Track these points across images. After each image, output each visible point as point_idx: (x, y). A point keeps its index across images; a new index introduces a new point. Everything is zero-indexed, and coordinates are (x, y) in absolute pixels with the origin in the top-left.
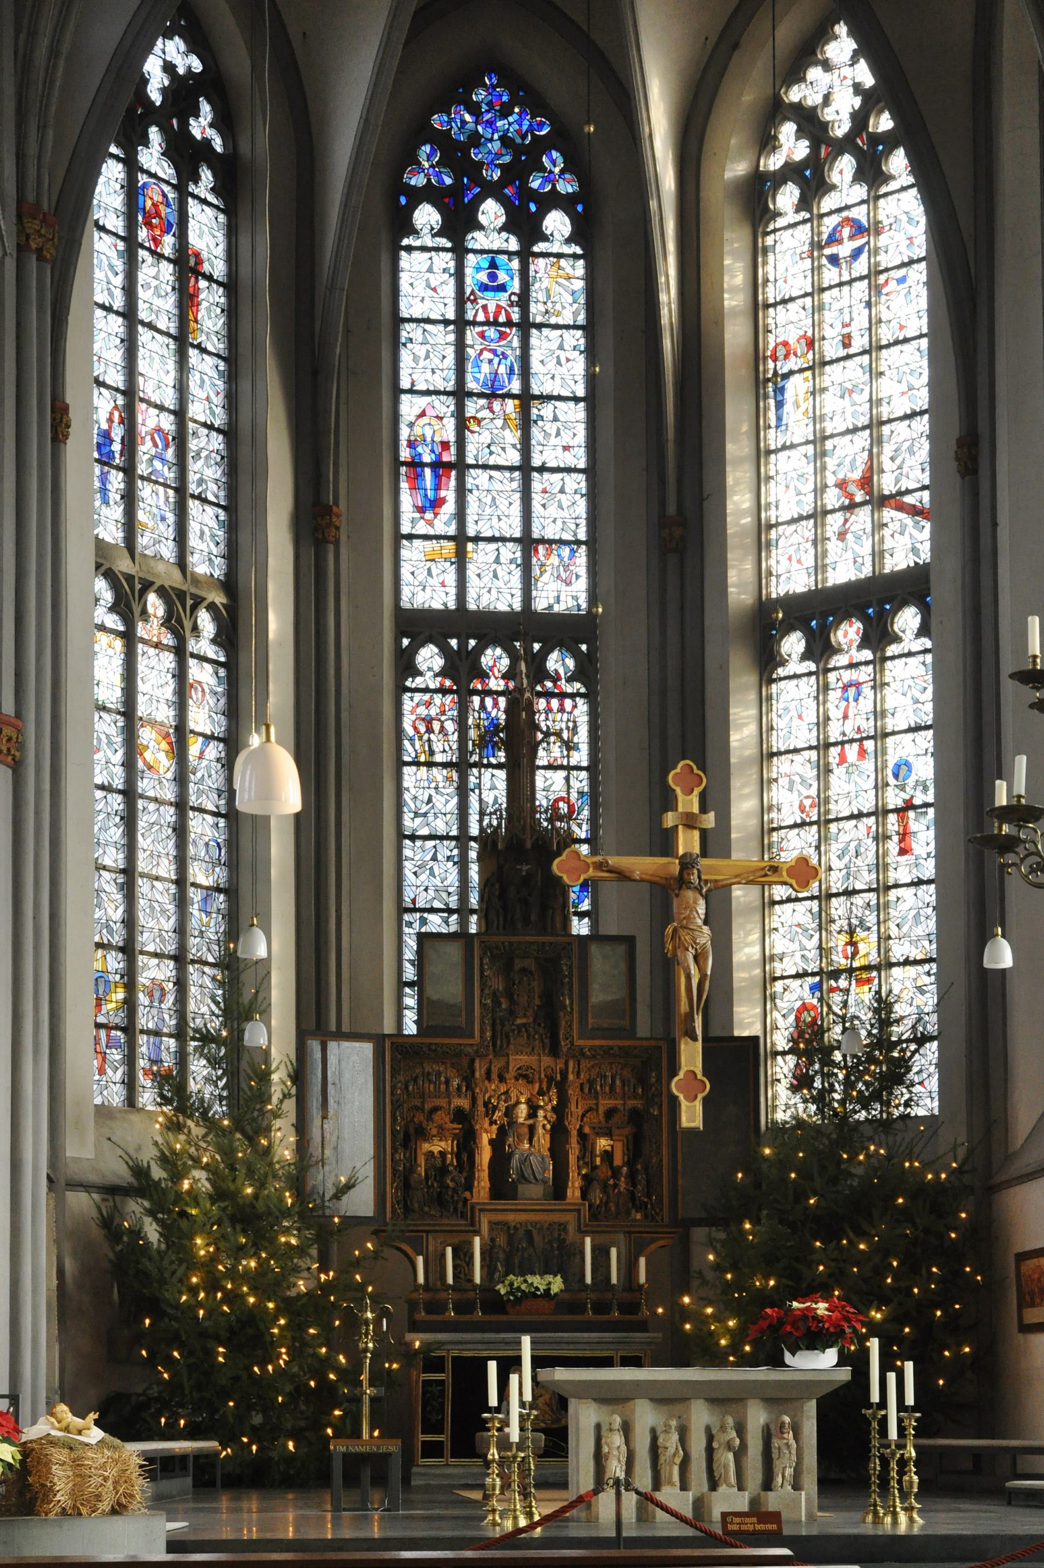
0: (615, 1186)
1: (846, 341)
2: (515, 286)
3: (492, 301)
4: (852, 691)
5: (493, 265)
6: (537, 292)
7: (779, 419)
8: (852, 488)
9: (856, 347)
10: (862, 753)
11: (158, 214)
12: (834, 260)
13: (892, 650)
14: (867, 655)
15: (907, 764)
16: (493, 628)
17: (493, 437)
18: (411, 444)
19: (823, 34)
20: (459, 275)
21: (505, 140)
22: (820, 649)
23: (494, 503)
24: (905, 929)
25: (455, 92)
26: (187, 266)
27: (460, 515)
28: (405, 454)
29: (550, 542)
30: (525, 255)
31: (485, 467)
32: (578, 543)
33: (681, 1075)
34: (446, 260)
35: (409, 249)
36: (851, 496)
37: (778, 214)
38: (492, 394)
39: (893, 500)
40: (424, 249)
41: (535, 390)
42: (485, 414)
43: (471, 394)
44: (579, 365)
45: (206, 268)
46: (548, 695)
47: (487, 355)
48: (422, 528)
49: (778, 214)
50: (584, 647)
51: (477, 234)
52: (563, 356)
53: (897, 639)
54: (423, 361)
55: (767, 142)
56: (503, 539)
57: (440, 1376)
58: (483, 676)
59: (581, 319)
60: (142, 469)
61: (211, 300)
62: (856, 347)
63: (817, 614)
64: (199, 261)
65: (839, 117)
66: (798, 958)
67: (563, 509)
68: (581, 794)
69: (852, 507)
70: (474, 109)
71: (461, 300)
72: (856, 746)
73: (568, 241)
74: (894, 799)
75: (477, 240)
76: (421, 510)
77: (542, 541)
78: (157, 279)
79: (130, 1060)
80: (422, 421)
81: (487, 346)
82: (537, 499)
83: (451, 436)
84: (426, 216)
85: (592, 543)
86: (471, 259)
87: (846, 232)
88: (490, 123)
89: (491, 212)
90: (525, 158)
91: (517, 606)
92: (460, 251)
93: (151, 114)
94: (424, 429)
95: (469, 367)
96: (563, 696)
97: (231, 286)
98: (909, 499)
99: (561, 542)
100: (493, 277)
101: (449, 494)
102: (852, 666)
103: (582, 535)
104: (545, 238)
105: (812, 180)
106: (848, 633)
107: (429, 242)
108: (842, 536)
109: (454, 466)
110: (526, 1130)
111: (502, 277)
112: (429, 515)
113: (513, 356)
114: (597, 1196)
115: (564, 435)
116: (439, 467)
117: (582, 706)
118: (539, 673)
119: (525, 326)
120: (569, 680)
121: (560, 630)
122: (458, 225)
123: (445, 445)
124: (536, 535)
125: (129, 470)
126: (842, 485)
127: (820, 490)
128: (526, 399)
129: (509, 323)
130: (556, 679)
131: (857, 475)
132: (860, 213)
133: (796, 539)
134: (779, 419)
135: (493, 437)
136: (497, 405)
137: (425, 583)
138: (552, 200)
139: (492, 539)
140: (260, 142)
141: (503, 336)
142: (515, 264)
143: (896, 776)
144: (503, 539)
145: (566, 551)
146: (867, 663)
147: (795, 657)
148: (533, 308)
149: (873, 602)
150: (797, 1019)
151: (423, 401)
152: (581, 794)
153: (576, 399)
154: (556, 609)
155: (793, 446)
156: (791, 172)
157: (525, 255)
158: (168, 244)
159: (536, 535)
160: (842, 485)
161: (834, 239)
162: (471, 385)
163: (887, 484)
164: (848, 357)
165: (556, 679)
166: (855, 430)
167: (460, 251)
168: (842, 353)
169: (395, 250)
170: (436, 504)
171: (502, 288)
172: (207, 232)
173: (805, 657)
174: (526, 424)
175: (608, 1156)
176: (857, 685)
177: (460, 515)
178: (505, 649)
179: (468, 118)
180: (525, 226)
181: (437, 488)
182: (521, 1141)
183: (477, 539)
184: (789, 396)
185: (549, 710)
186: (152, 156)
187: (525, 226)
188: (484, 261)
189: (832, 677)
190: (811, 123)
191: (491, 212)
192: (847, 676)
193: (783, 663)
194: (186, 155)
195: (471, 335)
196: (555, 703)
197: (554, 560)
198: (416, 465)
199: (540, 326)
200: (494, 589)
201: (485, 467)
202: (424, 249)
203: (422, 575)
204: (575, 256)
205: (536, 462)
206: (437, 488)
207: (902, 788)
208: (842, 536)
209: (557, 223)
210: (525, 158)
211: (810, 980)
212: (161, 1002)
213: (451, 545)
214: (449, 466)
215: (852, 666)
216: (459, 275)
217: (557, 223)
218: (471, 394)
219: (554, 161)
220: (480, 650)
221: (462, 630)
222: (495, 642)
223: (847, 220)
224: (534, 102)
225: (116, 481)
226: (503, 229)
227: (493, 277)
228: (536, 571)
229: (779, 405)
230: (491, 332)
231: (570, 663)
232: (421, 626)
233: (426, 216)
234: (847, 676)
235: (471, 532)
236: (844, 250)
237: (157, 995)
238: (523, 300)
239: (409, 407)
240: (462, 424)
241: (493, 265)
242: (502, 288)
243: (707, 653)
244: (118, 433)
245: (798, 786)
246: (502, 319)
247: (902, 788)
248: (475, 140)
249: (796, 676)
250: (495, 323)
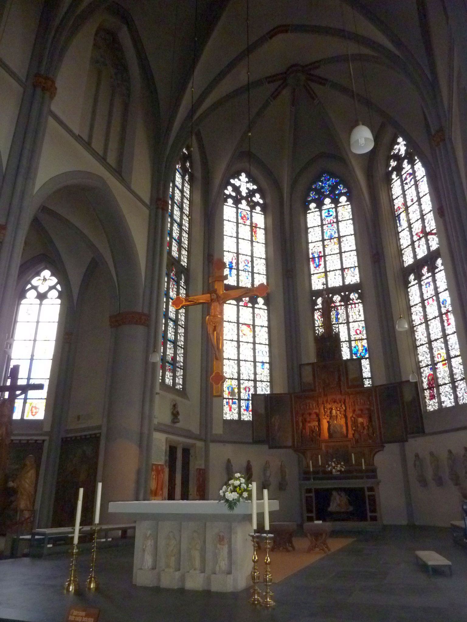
0: (363, 432)
1: (412, 200)
2: (334, 214)
3: (329, 219)
4: (428, 285)
5: (329, 211)
6: (339, 214)
7: (400, 224)
8: (419, 234)
9: (415, 201)
10: (433, 300)
11: (245, 217)
12: (406, 184)
13: (437, 270)
14: (430, 274)
15: (446, 300)
16: (335, 291)
17: (332, 247)
18: (312, 254)
19: (396, 138)
20: (321, 215)
21: (329, 186)
22: (419, 277)
23: (333, 263)
24: (453, 347)
25: (318, 179)
26: (253, 227)
27: (325, 267)
28: (311, 256)
29: (348, 268)
30: (336, 208)
31: (330, 255)
32: (355, 267)
33: (214, 374)
34: (318, 213)
35: (309, 213)
36: (419, 236)
37: (393, 179)
38: (331, 238)
39: (430, 233)
40: (312, 212)
41: (341, 235)
42: (330, 243)
43: (326, 240)
44: (352, 227)
45: (258, 226)
46: (351, 304)
47: (329, 230)
48: (316, 272)
49: (393, 179)
50: (360, 291)
51: (325, 206)
52: (347, 226)
53: (310, 209)
54: (314, 235)
55: (388, 165)
56: (336, 270)
57: (311, 495)
58: (334, 302)
59: (351, 217)
60: (241, 268)
61: (260, 235)
62: (415, 201)
63: (417, 268)
64: (256, 224)
65: (403, 152)
66: (425, 361)
67: (351, 259)
68: (363, 327)
69: (420, 239)
70: (322, 182)
71: (322, 220)
72: (431, 299)
73: (346, 202)
74: (444, 310)
75: (325, 207)
76: (316, 268)
77: (346, 268)
78: (245, 231)
79: (240, 407)
80: (314, 248)
81: (332, 238)
82: (344, 259)
83: (321, 250)
84: (313, 205)
85: (359, 266)
86: (323, 212)
87: (408, 176)
88: (326, 183)
89: (327, 201)
90: (334, 188)
91: (341, 284)
92: (321, 211)
93: (243, 198)
94: (315, 250)
95: (325, 234)
96: (355, 304)
97: (265, 229)
98: (433, 232)
99: (351, 268)
100: (329, 214)
101: (322, 263)
102: (427, 278)
103: (356, 265)
104: (340, 203)
105: (399, 169)
106: (425, 270)
107: (313, 210)
108: (419, 247)
109: (323, 256)
110: (335, 417)
111: (331, 213)
112: (317, 268)
113: (335, 229)
114: (357, 436)
115: (349, 243)
116: (320, 257)
117: (361, 305)
118: (349, 299)
119: (338, 222)
120: (357, 300)
121: (352, 288)
122: (320, 205)
123: (320, 252)
124: (344, 267)
125: (238, 270)
126: (417, 234)
127: (412, 236)
128: (339, 238)
129: (334, 222)
130: (353, 300)
131: (420, 230)
132: (411, 171)
133: (408, 251)
134: (400, 224)
135: (332, 247)
136: (332, 240)
137: (317, 284)
138: (341, 194)
139: (334, 270)
140: (268, 200)
141: (332, 225)
142: (334, 210)
143: (443, 304)
144: (336, 270)
145: (352, 269)
146: (430, 276)
147: (412, 280)
148: (339, 218)
149: (429, 261)
150: (428, 378)
151: (314, 244)
152: (363, 327)
153: (352, 235)
154: (351, 283)
155: (404, 229)
156: (394, 169)
157: (336, 208)
158: (248, 222)
159: (344, 267)
160: (417, 234)
161: (406, 179)
162: (326, 238)
163: (428, 230)
164: (413, 204)
165: (353, 300)
166: (418, 220)
167: (321, 211)
168: (412, 203)
169: (305, 214)
170: (319, 265)
171: (331, 215)
172: (259, 219)
173: (414, 280)
174: (340, 243)
175: (362, 424)
176: (429, 283)
177: (325, 267)
178: (339, 295)
179: (320, 184)
180: (335, 202)
181: (319, 262)
182: (334, 421)
183: (330, 271)
184: (401, 218)
185: (352, 308)
186: (244, 205)
187: (335, 202)
188: (327, 211)
189: (422, 283)
190: (397, 157)
191: (327, 201)
192: (426, 281)
193: (410, 283)
194: (253, 206)
195: (325, 227)
196: (353, 306)
197: (350, 271)
198: (314, 258)
199: (341, 221)
200: (335, 281)
201: (330, 255)
202: (312, 212)
203: (317, 282)
204: (348, 205)
205: (343, 251)
206: (319, 262)
207: (445, 307)
208: (419, 247)
209: (343, 199)
210: (334, 188)
211: (430, 367)
212: (249, 391)
213: (324, 274)
214: (322, 256)
215: (427, 278)
216: (321, 215)
217: (343, 199)
218: (326, 240)
219: (341, 187)
220: (332, 297)
221: (328, 292)
222: (335, 294)
223: (408, 174)
224: (333, 175)
225: (234, 272)
226: (330, 203)
227: (329, 214)
228: (345, 275)
229: (400, 221)
230: (330, 225)
231: (357, 295)
232: (318, 293)
233: (313, 205)
234: (426, 281)
235: (328, 270)
236: (408, 181)
237: (247, 390)
238: (337, 217)
239: (311, 246)
240: (324, 247)
241: (329, 211)
242: (331, 215)
243: (10, 144)
244: (234, 262)
245: (418, 314)
246: (332, 222)
247: (445, 307)
248: (322, 188)
249: (414, 285)
250: (330, 223)
